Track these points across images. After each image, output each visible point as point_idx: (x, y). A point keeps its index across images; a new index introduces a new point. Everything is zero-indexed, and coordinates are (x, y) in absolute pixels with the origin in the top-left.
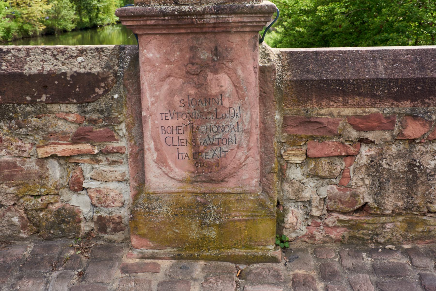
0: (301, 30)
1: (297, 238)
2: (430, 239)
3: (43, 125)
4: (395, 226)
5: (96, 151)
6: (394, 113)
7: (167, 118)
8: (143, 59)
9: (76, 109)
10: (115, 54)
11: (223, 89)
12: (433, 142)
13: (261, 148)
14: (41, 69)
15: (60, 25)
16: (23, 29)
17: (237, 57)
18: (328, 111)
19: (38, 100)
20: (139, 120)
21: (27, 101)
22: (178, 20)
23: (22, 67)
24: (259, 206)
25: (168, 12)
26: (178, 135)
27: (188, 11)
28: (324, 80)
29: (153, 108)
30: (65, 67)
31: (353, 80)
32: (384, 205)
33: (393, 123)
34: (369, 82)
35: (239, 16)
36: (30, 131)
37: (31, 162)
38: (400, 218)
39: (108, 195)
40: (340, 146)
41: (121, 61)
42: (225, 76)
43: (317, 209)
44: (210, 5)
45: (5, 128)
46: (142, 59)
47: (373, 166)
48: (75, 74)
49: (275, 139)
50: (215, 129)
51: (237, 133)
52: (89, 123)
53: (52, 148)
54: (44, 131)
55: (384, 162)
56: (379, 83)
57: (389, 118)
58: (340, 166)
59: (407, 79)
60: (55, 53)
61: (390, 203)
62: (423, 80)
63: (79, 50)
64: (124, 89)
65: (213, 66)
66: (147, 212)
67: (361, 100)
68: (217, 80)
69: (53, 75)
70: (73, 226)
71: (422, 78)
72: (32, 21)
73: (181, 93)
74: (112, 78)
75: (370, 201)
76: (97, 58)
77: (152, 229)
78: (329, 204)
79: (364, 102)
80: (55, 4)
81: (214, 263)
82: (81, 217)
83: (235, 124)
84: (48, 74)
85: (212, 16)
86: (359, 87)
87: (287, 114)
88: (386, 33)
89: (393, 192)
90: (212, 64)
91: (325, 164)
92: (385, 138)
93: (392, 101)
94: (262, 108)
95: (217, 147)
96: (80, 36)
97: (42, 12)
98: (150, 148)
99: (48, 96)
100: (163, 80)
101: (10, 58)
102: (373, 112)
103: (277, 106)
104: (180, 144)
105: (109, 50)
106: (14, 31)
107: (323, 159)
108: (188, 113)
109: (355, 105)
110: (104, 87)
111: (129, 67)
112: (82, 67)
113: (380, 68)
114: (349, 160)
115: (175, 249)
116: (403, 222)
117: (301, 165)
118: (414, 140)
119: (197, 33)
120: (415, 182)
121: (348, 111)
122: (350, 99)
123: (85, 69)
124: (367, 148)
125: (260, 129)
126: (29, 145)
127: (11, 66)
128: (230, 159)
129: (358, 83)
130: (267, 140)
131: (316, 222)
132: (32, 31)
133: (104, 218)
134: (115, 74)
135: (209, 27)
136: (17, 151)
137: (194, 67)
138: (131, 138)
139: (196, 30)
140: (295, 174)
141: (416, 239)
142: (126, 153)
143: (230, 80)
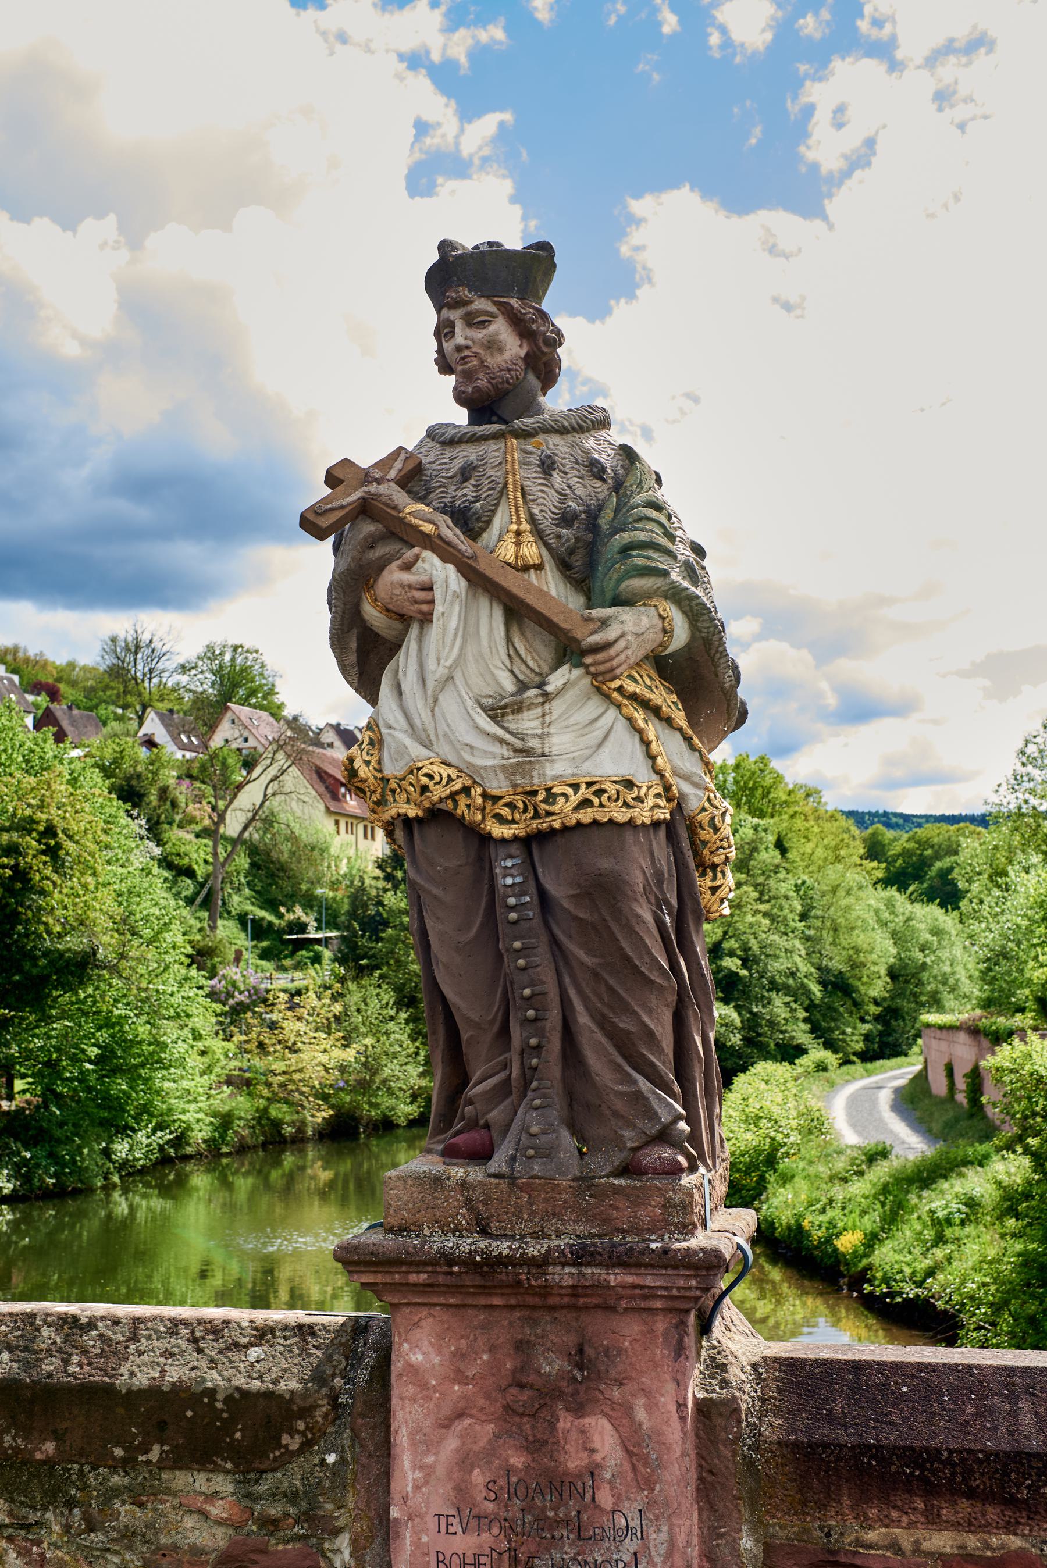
3: (147, 1527)
7: (451, 1529)
8: (399, 1365)
9: (230, 1488)
10: (341, 1344)
11: (598, 1457)
14: (157, 1375)
15: (376, 1106)
16: (268, 1119)
17: (634, 1375)
18: (886, 1535)
19: (140, 1458)
21: (114, 1458)
22: (483, 1275)
23: (114, 1369)
25: (459, 1256)
27: (507, 1256)
28: (870, 1447)
29: (419, 1498)
31: (951, 1452)
34: (994, 1461)
35: (633, 1270)
36: (113, 1540)
41: (352, 1365)
45: (57, 1528)
48: (237, 1395)
52: (259, 1528)
54: (147, 1542)
56: (1023, 1465)
60: (198, 1334)
63: (256, 1329)
64: (352, 1439)
65: (572, 1395)
67: (976, 1510)
68: (583, 1432)
69: (183, 1395)
72: (296, 1094)
73: (489, 1463)
74: (324, 1409)
76: (297, 1351)
79: (984, 1515)
80: (366, 1046)
83: (627, 1558)
85: (567, 1270)
86: (968, 1474)
87: (773, 1536)
90: (569, 1390)
94: (705, 1514)
97: (326, 1070)
99: (166, 1448)
100: (446, 1424)
101: (91, 1343)
102: (1013, 1547)
103: (746, 1513)
105: (328, 1332)
106: (242, 1123)
108: (506, 1520)
109: (959, 1524)
110: (303, 1433)
112: (255, 1375)
113: (1027, 1421)
119: (533, 1308)
122: (944, 1505)
123: (263, 1382)
127: (89, 1364)
129: (963, 1460)
132: (292, 1124)
134: (333, 1398)
135: (561, 1295)
137: (525, 1396)
139: (530, 1300)
143: (616, 1436)
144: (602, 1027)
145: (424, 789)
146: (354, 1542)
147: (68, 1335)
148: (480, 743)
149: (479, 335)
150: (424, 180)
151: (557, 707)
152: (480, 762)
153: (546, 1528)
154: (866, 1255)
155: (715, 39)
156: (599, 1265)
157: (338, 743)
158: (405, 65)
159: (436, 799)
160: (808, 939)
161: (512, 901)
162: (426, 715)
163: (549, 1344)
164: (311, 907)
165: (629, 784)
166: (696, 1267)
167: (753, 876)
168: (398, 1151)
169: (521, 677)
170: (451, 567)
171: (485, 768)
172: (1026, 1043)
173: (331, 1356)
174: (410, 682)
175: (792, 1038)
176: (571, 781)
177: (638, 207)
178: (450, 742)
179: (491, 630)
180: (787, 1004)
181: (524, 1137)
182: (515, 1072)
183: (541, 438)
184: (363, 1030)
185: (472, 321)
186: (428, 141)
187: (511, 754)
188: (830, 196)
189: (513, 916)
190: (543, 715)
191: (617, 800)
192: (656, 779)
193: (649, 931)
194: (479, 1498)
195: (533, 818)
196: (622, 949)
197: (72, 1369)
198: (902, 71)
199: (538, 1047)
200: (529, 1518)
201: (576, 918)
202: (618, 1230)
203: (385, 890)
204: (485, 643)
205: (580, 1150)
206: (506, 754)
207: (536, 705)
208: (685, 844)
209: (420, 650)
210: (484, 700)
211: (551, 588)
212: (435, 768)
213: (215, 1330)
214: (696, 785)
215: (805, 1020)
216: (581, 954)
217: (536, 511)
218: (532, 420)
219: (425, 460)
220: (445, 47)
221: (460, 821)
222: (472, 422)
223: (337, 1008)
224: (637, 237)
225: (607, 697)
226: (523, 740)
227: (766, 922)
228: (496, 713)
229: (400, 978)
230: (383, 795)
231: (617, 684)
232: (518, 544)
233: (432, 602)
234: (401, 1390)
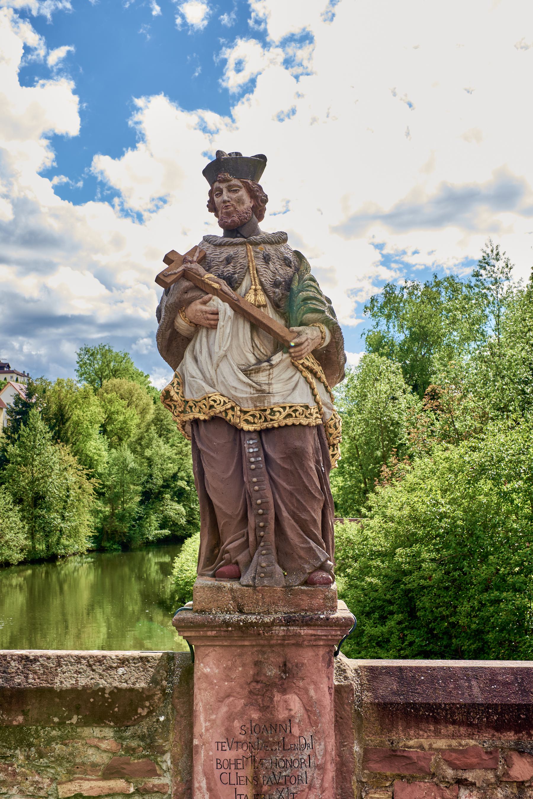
0: (374, 581)
3: (69, 755)
6: (496, 747)
7: (224, 748)
9: (112, 734)
10: (162, 665)
11: (293, 713)
13: (337, 788)
14: (74, 682)
17: (309, 675)
18: (417, 742)
20: (189, 751)
21: (54, 723)
26: (237, 771)
28: (411, 704)
29: (208, 735)
31: (445, 704)
36: (52, 762)
40: (435, 788)
44: (279, 615)
45: (21, 757)
46: (197, 674)
48: (115, 691)
49: (354, 778)
50: (282, 764)
52: (126, 753)
53: (77, 785)
57: (491, 753)
59: (508, 705)
60: (91, 663)
63: (119, 659)
64: (172, 709)
68: (286, 702)
69: (88, 691)
71: (525, 704)
83: (305, 757)
84: (82, 690)
85: (282, 628)
86: (453, 713)
88: (497, 590)
90: (280, 683)
92: (488, 780)
93: (492, 732)
95: (284, 787)
96: (29, 572)
98: (200, 787)
99: (80, 717)
100: (221, 701)
104: (239, 783)
105: (155, 660)
110: (148, 707)
111: (180, 682)
113: (476, 690)
118: (523, 783)
124: (467, 792)
125: (336, 764)
126: (48, 780)
127: (39, 678)
129: (451, 708)
130: (344, 779)
134: (163, 690)
136: (33, 788)
137: (259, 686)
138: (176, 773)
142: (169, 792)
144: (293, 518)
145: (211, 407)
146: (173, 757)
147: (25, 665)
149: (234, 196)
150: (27, 77)
155: (179, 21)
156: (297, 625)
158: (18, 15)
159: (218, 411)
161: (252, 460)
162: (212, 372)
163: (270, 662)
165: (307, 407)
166: (341, 626)
169: (258, 357)
171: (242, 398)
172: (343, 524)
173: (159, 671)
174: (203, 357)
176: (282, 405)
177: (140, 102)
178: (225, 385)
179: (244, 334)
181: (259, 568)
182: (251, 538)
183: (262, 246)
185: (230, 189)
186: (30, 57)
187: (255, 392)
188: (233, 106)
189: (253, 466)
190: (269, 375)
192: (315, 404)
194: (237, 733)
195: (264, 422)
196: (304, 482)
197: (30, 681)
198: (270, 47)
199: (264, 527)
200: (261, 741)
201: (283, 468)
202: (303, 610)
203: (8, 444)
204: (241, 340)
207: (266, 370)
209: (208, 342)
210: (240, 367)
211: (270, 315)
213: (100, 661)
216: (285, 484)
219: (208, 252)
220: (39, 9)
221: (227, 423)
222: (225, 235)
224: (138, 117)
225: (297, 368)
226: (260, 385)
228: (247, 372)
230: (184, 408)
232: (256, 295)
233: (218, 320)
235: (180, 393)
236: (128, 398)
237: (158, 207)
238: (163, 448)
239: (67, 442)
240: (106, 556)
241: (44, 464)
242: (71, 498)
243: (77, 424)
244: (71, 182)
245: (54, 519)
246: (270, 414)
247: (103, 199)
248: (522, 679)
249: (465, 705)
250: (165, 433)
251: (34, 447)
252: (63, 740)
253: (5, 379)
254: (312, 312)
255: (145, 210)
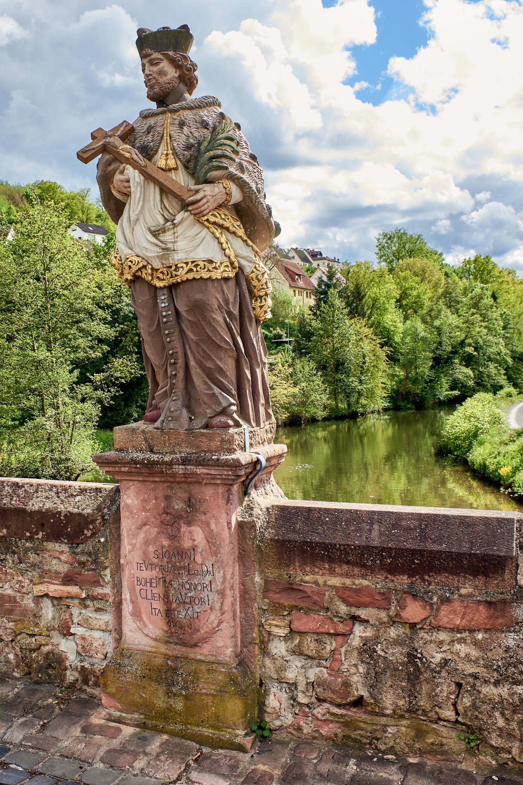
1: (281, 727)
2: (443, 755)
4: (398, 731)
5: (84, 595)
6: (389, 589)
9: (67, 550)
11: (196, 543)
12: (438, 630)
18: (313, 578)
20: (118, 569)
21: (26, 536)
22: (149, 469)
24: (230, 681)
26: (152, 588)
28: (307, 542)
29: (130, 556)
30: (62, 506)
31: (340, 545)
32: (382, 701)
33: (388, 600)
36: (28, 567)
37: (28, 599)
38: (404, 722)
39: (91, 644)
42: (199, 529)
43: (303, 695)
47: (367, 650)
50: (187, 586)
51: (210, 593)
55: (379, 647)
58: (330, 645)
59: (402, 549)
61: (389, 700)
62: (421, 553)
63: (80, 489)
66: (117, 669)
68: (190, 533)
70: (58, 672)
71: (420, 550)
73: (155, 543)
75: (364, 694)
77: (120, 689)
78: (318, 690)
81: (177, 740)
82: (68, 664)
83: (207, 582)
85: (181, 467)
86: (347, 554)
87: (268, 577)
89: (391, 686)
90: (185, 516)
91: (311, 641)
93: (385, 574)
94: (241, 567)
96: (334, 427)
100: (140, 527)
103: (257, 567)
104: (153, 598)
107: (309, 635)
113: (375, 533)
114: (340, 639)
115: (142, 716)
116: (408, 727)
117: (286, 639)
118: (415, 624)
120: (417, 678)
121: (335, 581)
128: (203, 622)
129: (345, 549)
130: (247, 605)
131: (304, 712)
133: (87, 669)
137: (168, 518)
140: (279, 648)
141: (424, 753)
148: (149, 246)
149: (155, 69)
151: (180, 230)
152: (150, 254)
153: (176, 570)
154: (512, 477)
157: (296, 257)
160: (507, 338)
161: (164, 314)
163: (177, 497)
164: (284, 328)
165: (211, 262)
167: (481, 310)
168: (318, 431)
169: (167, 217)
170: (136, 171)
171: (151, 257)
175: (498, 382)
179: (155, 197)
180: (496, 367)
183: (181, 112)
184: (303, 380)
191: (204, 268)
192: (226, 259)
193: (220, 325)
194: (152, 557)
196: (207, 333)
197: (13, 502)
199: (176, 375)
201: (188, 320)
205: (190, 418)
206: (159, 251)
207: (171, 229)
208: (245, 287)
211: (181, 179)
212: (133, 258)
213: (65, 489)
214: (250, 262)
215: (504, 374)
217: (175, 145)
218: (177, 104)
219: (135, 126)
223: (291, 370)
224: (427, 16)
227: (486, 331)
228: (156, 233)
229: (319, 358)
231: (206, 218)
232: (167, 160)
233: (130, 187)
234: (124, 514)
235: (118, 258)
236: (422, 275)
237: (450, 98)
238: (451, 318)
239: (363, 316)
240: (402, 413)
241: (343, 336)
242: (367, 365)
243: (375, 300)
244: (370, 86)
245: (352, 382)
246: (175, 270)
247: (399, 98)
248: (426, 525)
249: (359, 547)
250: (454, 304)
251: (333, 321)
252: (37, 551)
253: (318, 265)
254: (217, 170)
255: (438, 102)
